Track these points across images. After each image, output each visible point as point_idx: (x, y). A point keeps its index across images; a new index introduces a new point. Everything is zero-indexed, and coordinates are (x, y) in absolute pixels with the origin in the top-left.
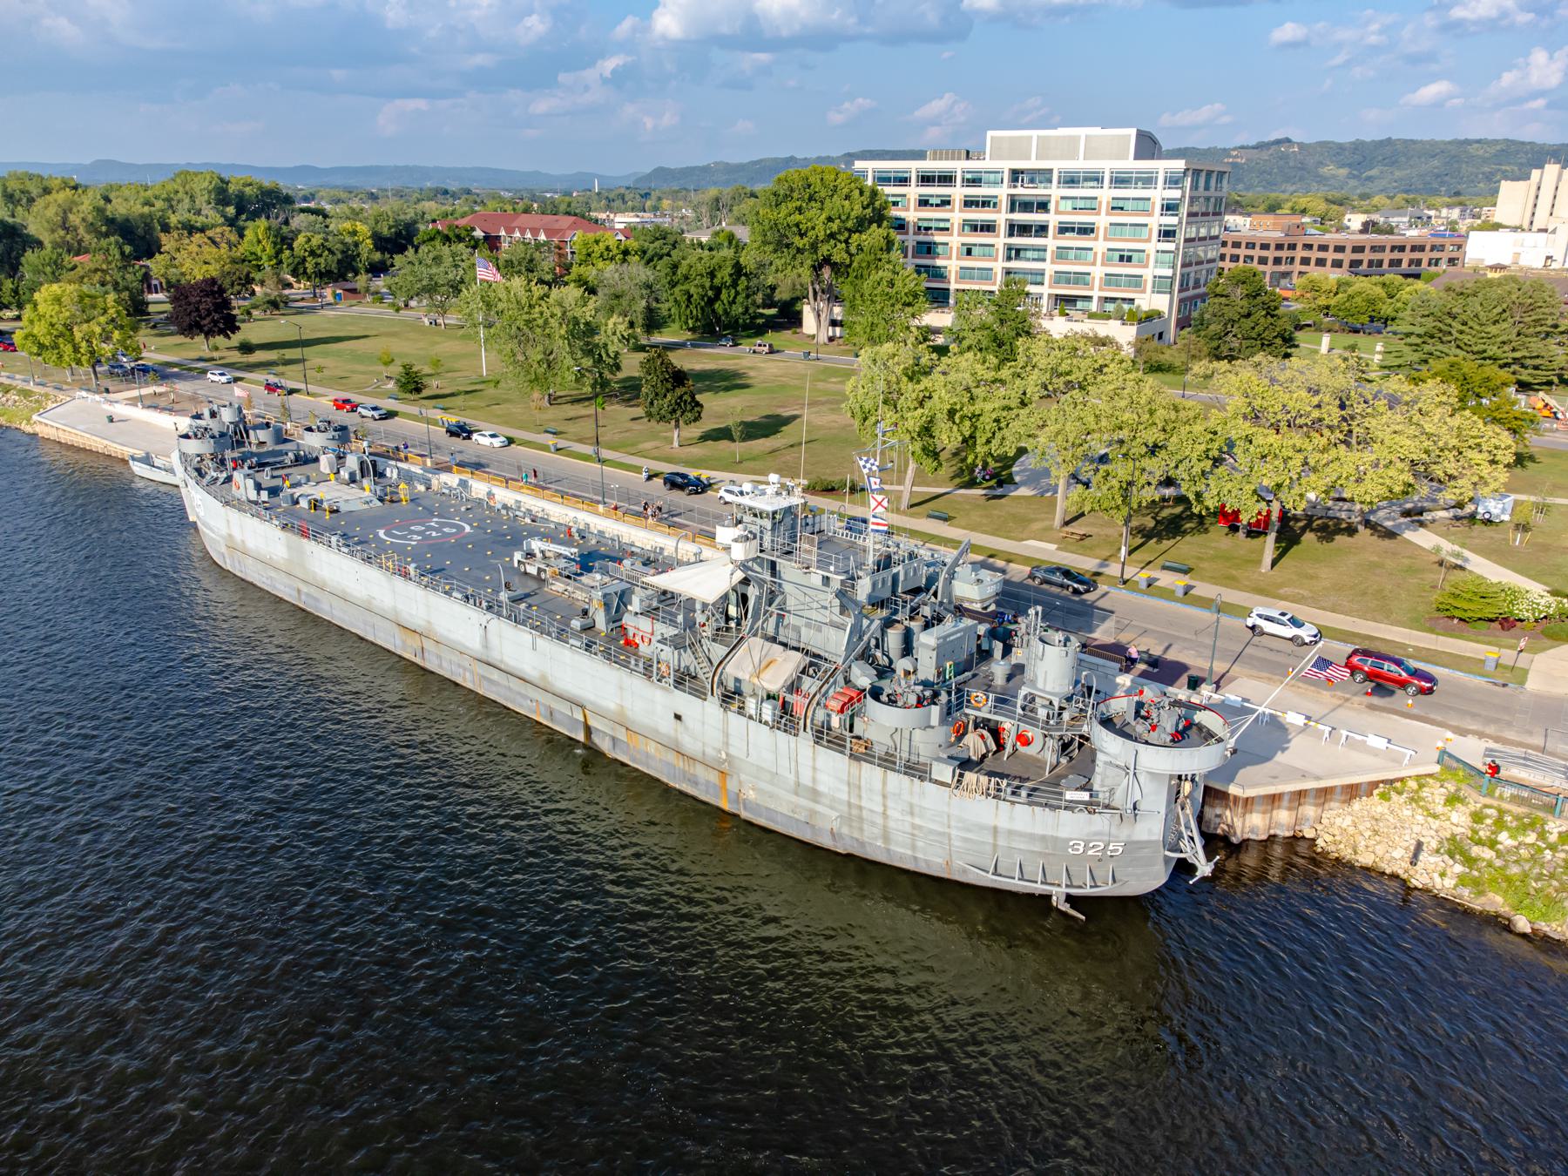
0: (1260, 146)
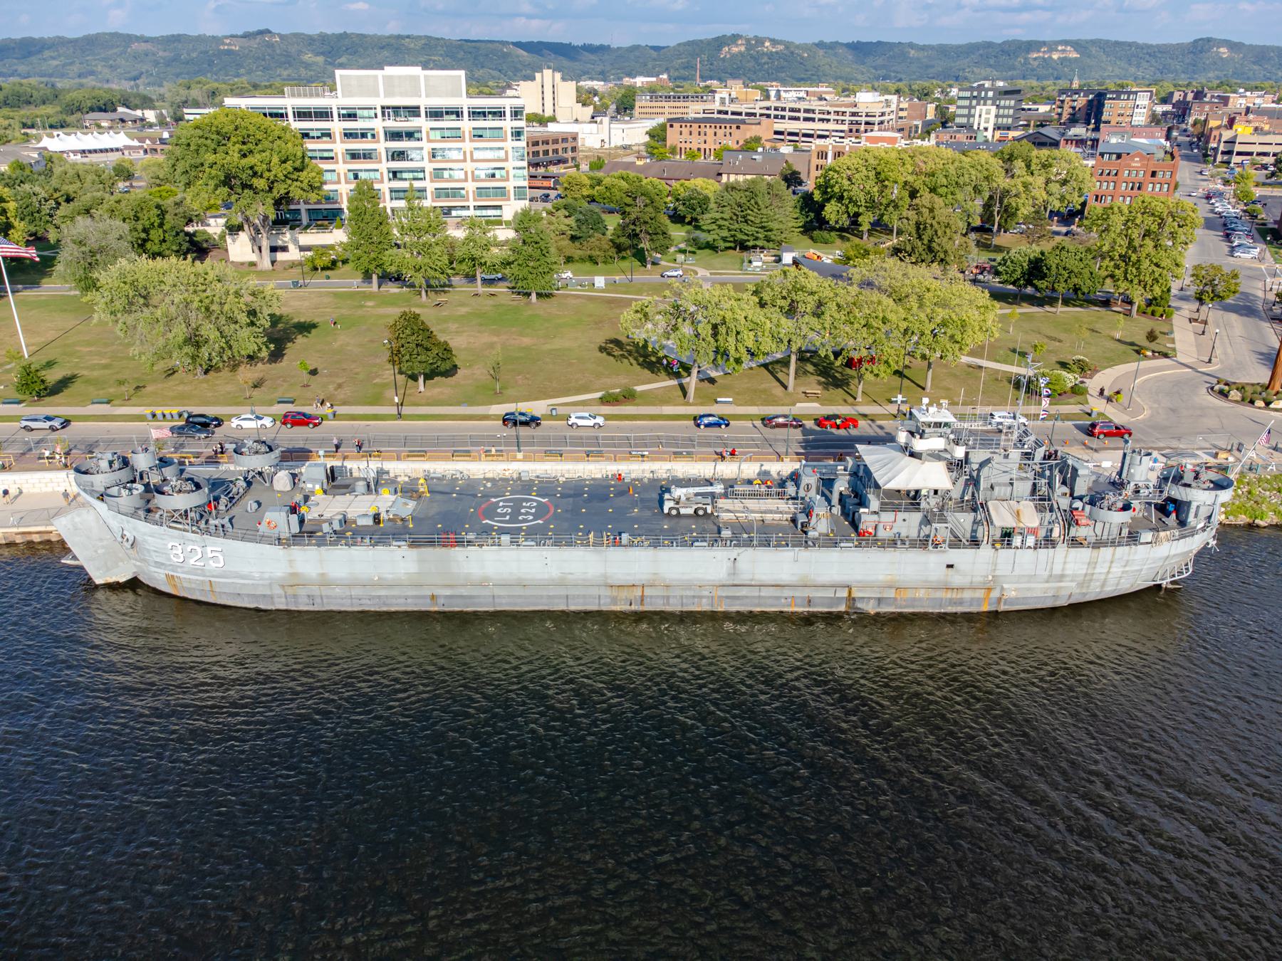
0: (246, 36)
